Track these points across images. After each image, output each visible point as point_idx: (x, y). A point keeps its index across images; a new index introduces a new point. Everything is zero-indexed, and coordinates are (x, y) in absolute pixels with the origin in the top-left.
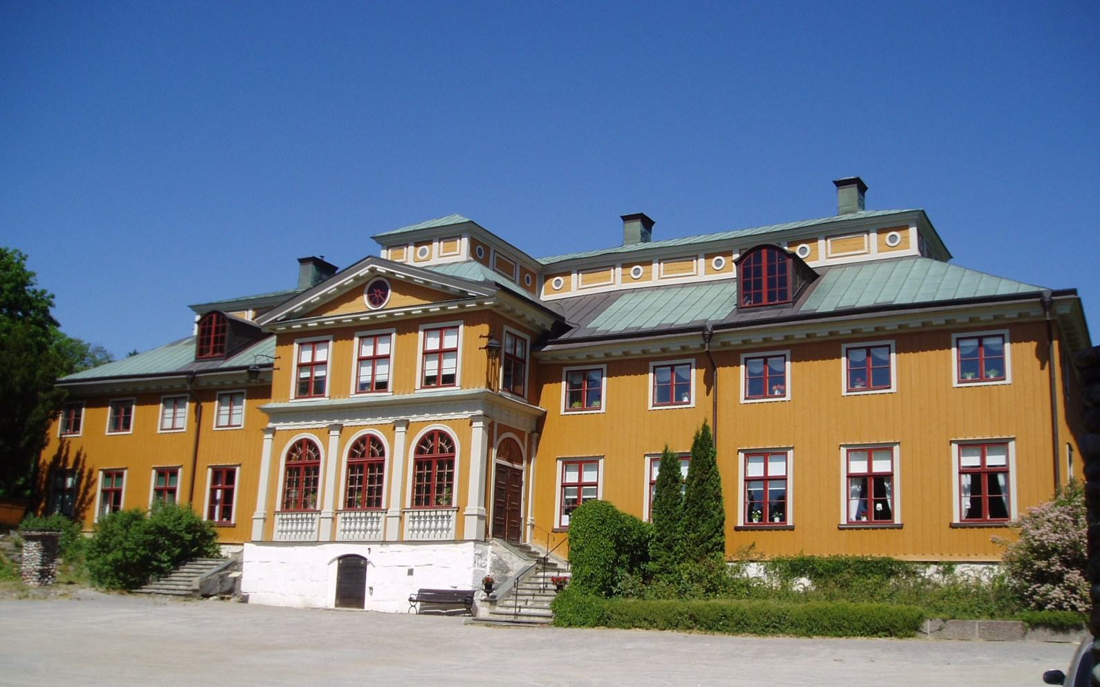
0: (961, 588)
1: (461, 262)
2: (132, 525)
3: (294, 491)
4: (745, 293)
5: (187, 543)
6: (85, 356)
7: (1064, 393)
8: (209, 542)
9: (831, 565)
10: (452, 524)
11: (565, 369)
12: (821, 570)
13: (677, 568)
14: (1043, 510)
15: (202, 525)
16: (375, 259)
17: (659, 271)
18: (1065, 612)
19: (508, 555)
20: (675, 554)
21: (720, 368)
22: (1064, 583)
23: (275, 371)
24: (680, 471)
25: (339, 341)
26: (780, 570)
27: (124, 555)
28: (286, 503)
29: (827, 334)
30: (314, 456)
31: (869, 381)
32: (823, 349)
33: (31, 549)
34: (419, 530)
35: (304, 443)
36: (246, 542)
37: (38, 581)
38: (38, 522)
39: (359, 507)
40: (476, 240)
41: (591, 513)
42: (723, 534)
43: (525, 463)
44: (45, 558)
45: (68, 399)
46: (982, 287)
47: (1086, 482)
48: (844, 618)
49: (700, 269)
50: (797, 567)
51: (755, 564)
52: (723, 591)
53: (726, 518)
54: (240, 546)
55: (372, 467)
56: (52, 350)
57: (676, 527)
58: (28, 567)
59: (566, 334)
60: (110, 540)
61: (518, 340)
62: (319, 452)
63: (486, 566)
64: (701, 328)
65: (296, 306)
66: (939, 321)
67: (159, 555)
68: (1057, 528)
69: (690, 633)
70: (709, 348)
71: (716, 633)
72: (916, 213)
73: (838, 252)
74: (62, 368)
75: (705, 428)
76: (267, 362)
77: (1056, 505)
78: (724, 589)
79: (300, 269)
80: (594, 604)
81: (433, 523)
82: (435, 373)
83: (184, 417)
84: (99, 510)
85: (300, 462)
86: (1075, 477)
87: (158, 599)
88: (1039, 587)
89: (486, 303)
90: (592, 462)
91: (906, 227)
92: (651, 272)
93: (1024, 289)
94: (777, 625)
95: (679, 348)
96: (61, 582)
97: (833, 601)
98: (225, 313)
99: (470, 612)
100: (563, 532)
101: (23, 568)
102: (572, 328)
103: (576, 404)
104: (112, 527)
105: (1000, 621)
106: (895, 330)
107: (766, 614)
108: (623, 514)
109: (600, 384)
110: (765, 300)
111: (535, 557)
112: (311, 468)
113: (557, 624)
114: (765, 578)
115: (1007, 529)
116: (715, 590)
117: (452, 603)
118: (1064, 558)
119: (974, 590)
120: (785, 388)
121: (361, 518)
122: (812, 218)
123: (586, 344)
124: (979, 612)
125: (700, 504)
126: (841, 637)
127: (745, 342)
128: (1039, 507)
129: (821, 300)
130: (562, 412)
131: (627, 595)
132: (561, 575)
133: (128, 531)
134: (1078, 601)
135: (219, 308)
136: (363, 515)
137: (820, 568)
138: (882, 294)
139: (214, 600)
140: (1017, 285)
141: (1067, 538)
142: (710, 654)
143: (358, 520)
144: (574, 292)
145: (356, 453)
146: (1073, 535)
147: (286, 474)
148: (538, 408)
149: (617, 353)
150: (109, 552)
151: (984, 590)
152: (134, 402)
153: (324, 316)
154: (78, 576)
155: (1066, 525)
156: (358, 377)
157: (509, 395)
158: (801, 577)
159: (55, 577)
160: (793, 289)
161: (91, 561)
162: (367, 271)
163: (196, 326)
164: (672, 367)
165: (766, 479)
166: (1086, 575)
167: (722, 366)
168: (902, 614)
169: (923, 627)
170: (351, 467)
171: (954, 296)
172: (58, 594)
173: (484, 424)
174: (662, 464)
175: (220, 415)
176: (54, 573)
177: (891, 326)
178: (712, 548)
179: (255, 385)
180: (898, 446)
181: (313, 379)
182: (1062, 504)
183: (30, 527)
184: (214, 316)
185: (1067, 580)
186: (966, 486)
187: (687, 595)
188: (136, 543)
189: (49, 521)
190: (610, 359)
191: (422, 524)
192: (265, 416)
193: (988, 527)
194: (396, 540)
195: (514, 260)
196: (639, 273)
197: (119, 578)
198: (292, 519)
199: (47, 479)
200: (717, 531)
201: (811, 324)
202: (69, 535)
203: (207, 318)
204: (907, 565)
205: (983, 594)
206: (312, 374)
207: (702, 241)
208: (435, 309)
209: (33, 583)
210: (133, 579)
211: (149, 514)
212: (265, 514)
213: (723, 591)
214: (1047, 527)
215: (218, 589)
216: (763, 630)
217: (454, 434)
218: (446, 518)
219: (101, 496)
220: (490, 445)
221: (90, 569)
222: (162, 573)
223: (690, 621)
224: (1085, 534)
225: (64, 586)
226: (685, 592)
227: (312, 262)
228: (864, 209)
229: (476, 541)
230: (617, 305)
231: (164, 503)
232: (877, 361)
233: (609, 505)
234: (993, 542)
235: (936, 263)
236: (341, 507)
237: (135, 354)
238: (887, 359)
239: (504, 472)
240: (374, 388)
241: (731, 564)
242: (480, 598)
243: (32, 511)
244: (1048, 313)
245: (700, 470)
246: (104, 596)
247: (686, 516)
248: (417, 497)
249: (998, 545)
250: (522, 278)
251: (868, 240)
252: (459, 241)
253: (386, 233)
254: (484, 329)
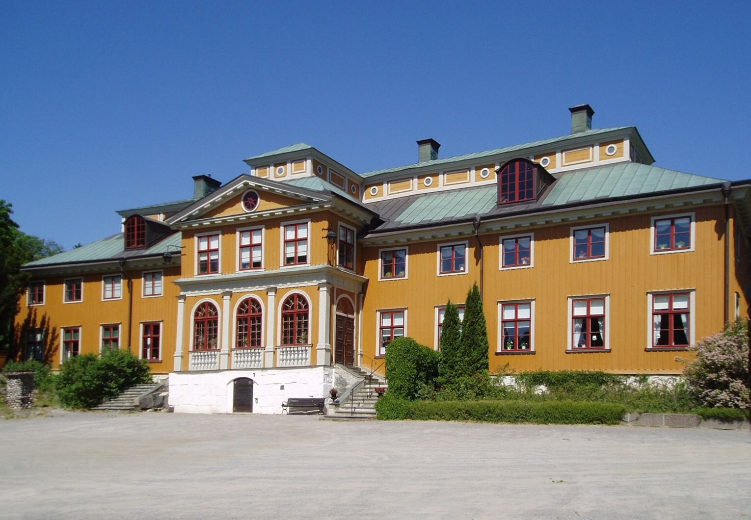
0: (652, 392)
1: (307, 177)
2: (88, 364)
3: (201, 337)
4: (503, 193)
5: (129, 375)
6: (42, 248)
7: (735, 256)
8: (144, 373)
9: (561, 377)
10: (309, 356)
11: (380, 250)
12: (553, 380)
13: (457, 380)
14: (715, 338)
15: (138, 362)
16: (247, 176)
17: (444, 180)
18: (730, 409)
19: (346, 375)
20: (456, 371)
21: (486, 246)
22: (730, 389)
23: (182, 257)
24: (458, 316)
25: (226, 235)
26: (526, 380)
27: (84, 384)
28: (196, 345)
29: (560, 221)
30: (214, 313)
31: (589, 252)
32: (556, 231)
33: (13, 384)
34: (286, 360)
35: (206, 305)
36: (171, 372)
37: (21, 406)
38: (17, 366)
39: (246, 346)
40: (316, 161)
41: (400, 346)
42: (487, 358)
43: (355, 314)
44: (25, 390)
45: (31, 279)
46: (676, 182)
47: (749, 319)
48: (569, 412)
49: (472, 178)
50: (537, 379)
51: (509, 377)
52: (488, 395)
53: (490, 347)
54: (166, 375)
55: (253, 319)
56: (15, 244)
57: (456, 354)
58: (11, 397)
59: (380, 226)
60: (73, 375)
61: (348, 231)
62: (217, 310)
63: (332, 382)
64: (473, 220)
65: (194, 211)
66: (642, 208)
67: (109, 384)
68: (725, 351)
69: (466, 422)
70: (478, 233)
71: (483, 422)
72: (631, 129)
73: (570, 162)
74: (24, 257)
75: (475, 287)
76: (176, 250)
77: (725, 335)
78: (488, 393)
79: (195, 184)
80: (403, 404)
81: (296, 355)
82: (293, 255)
83: (120, 289)
84: (63, 355)
85: (204, 317)
86: (740, 316)
87: (111, 413)
88: (710, 392)
89: (325, 206)
90: (400, 312)
91: (621, 141)
92: (438, 181)
93: (709, 181)
94: (524, 417)
95: (457, 234)
96: (39, 406)
97: (562, 401)
98: (143, 216)
99: (323, 412)
100: (382, 359)
101: (8, 398)
102: (384, 222)
103: (388, 274)
104: (74, 367)
105: (680, 414)
106: (610, 216)
107: (517, 409)
108: (421, 346)
109: (404, 260)
110: (517, 199)
111: (363, 375)
112: (212, 321)
113: (379, 418)
114: (516, 386)
115: (687, 352)
116: (483, 394)
117: (310, 407)
118: (729, 372)
119: (662, 393)
120: (530, 259)
121: (248, 353)
122: (552, 137)
123: (394, 233)
124: (665, 408)
125: (472, 338)
126: (567, 424)
127: (502, 228)
128: (712, 337)
129: (557, 197)
130: (379, 280)
131: (425, 398)
132: (381, 386)
133: (85, 369)
134: (740, 401)
135: (138, 213)
136: (249, 351)
137: (553, 379)
138: (601, 191)
139: (150, 411)
140: (704, 179)
141: (732, 358)
142: (480, 436)
143: (246, 355)
144: (386, 197)
145: (242, 311)
146: (737, 356)
147: (195, 326)
148: (363, 277)
149: (415, 238)
150: (72, 383)
151: (669, 393)
152: (82, 280)
153: (214, 217)
154: (51, 401)
155: (732, 349)
156: (240, 259)
157: (344, 269)
158: (540, 385)
159: (33, 402)
160: (537, 189)
161: (59, 390)
162: (242, 185)
163: (123, 225)
164: (453, 247)
165: (516, 321)
166: (747, 384)
167: (487, 246)
168: (610, 409)
169: (624, 418)
170: (239, 320)
171: (655, 190)
172: (37, 414)
173: (327, 289)
174: (446, 313)
175: (145, 287)
176: (32, 400)
177: (607, 213)
178: (480, 367)
179: (168, 266)
180: (609, 296)
181: (210, 261)
182: (730, 334)
183: (11, 369)
184: (136, 218)
185: (732, 387)
186: (657, 323)
187: (464, 398)
188: (92, 377)
189: (25, 365)
190: (411, 243)
191: (289, 356)
192: (178, 288)
193: (673, 351)
194: (271, 367)
195: (344, 175)
196: (430, 182)
197: (81, 401)
198: (201, 356)
199: (21, 336)
200: (483, 356)
201: (549, 214)
202: (41, 374)
203: (131, 220)
204: (613, 376)
205: (668, 396)
206: (208, 258)
207: (473, 157)
208: (291, 211)
209: (16, 407)
210: (91, 401)
211: (100, 356)
212: (182, 353)
213: (488, 395)
214: (717, 351)
215: (152, 404)
216: (515, 420)
217: (308, 295)
218: (304, 352)
219: (63, 346)
220: (332, 303)
221: (59, 396)
222: (112, 395)
223: (467, 414)
224: (746, 356)
225: (41, 408)
226: (463, 395)
227: (203, 179)
228: (590, 129)
229: (325, 366)
230: (414, 205)
231: (111, 348)
232: (596, 238)
233: (411, 340)
234: (677, 361)
235: (642, 166)
236: (234, 346)
237: (80, 246)
238: (603, 236)
239: (342, 320)
240: (252, 266)
241: (493, 377)
242: (328, 403)
243: (12, 358)
244: (727, 199)
245: (472, 315)
246: (71, 413)
247: (463, 346)
248: (284, 338)
249: (680, 363)
250: (349, 187)
251: (593, 151)
252: (305, 162)
253: (253, 158)
254: (325, 224)
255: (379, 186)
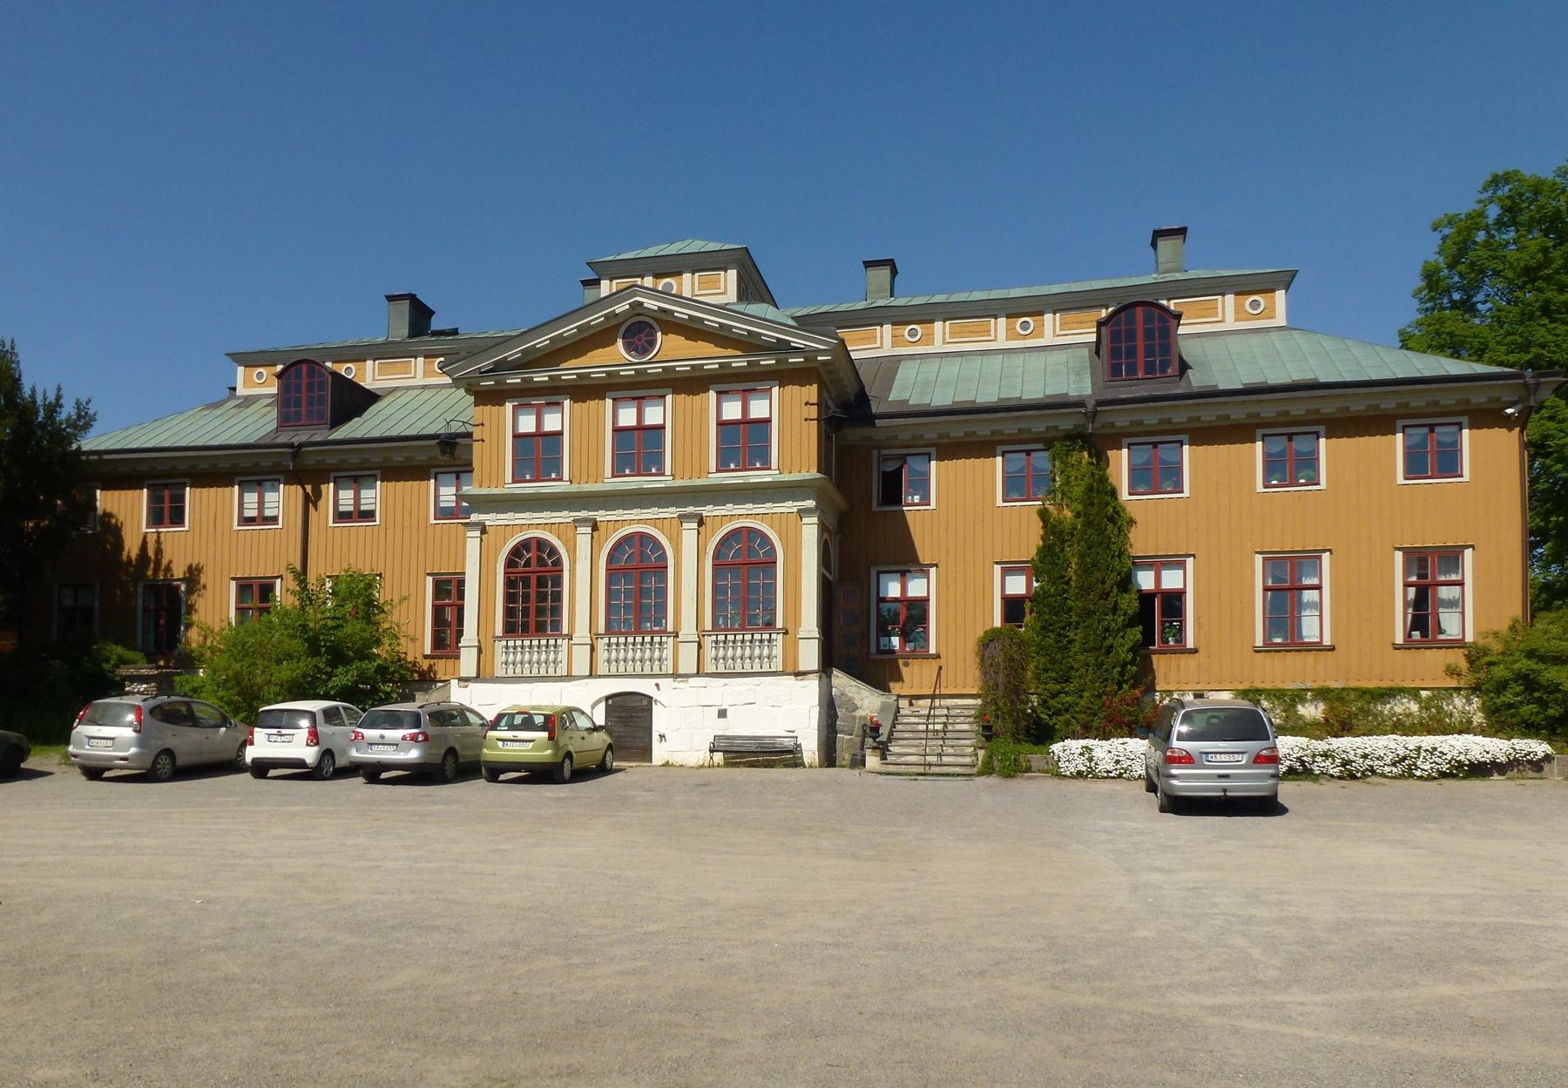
10: (778, 650)
17: (944, 334)
49: (1051, 328)
92: (933, 334)
149: (957, 433)
153: (563, 366)
162: (628, 307)
208: (739, 363)
255: (338, 371)
